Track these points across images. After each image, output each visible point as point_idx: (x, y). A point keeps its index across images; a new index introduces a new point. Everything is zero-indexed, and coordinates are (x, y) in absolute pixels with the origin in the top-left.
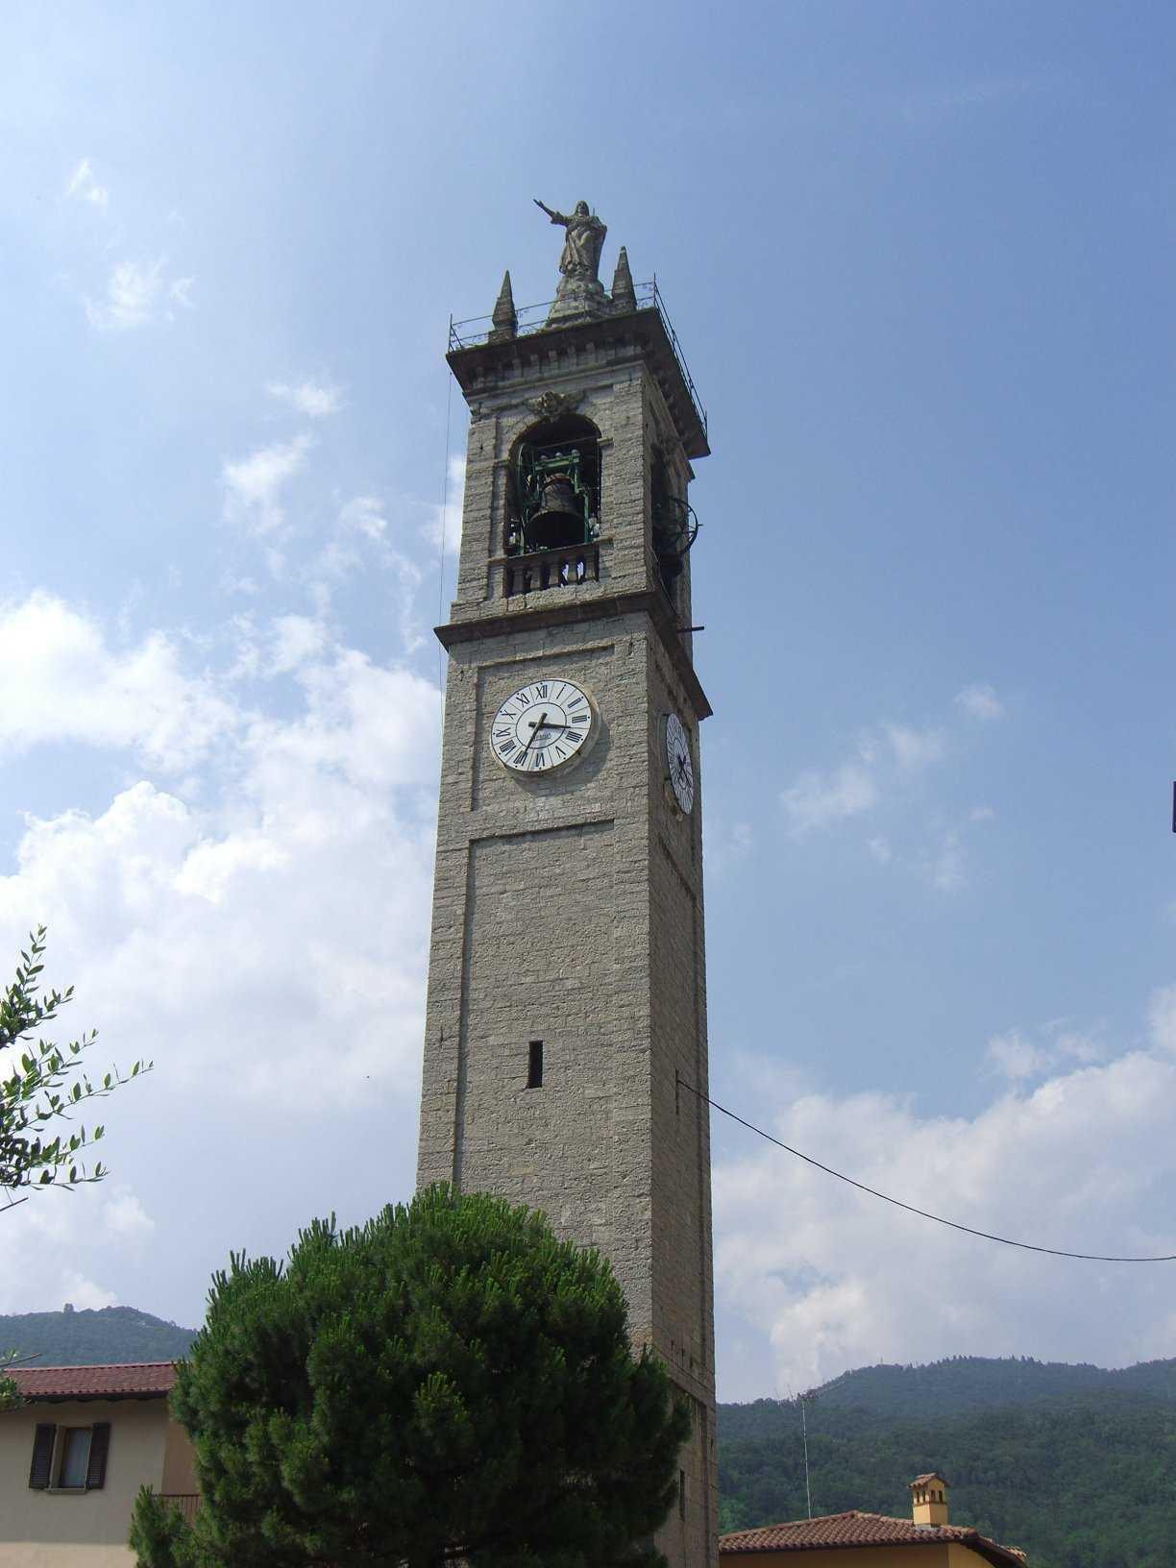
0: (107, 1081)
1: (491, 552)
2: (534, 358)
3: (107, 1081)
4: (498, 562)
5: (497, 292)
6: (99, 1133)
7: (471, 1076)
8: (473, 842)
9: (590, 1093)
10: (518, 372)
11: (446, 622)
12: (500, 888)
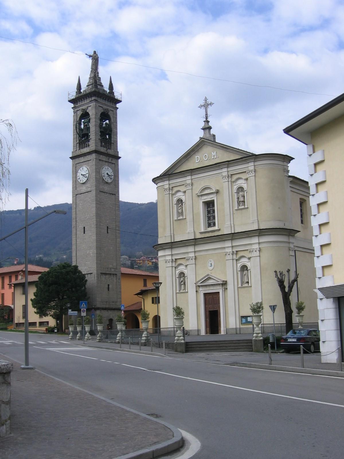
0: (314, 446)
1: (77, 142)
2: (80, 100)
3: (314, 446)
4: (78, 143)
5: (77, 82)
6: (2, 120)
7: (78, 232)
8: (76, 195)
9: (90, 234)
10: (79, 103)
11: (71, 156)
12: (79, 202)
